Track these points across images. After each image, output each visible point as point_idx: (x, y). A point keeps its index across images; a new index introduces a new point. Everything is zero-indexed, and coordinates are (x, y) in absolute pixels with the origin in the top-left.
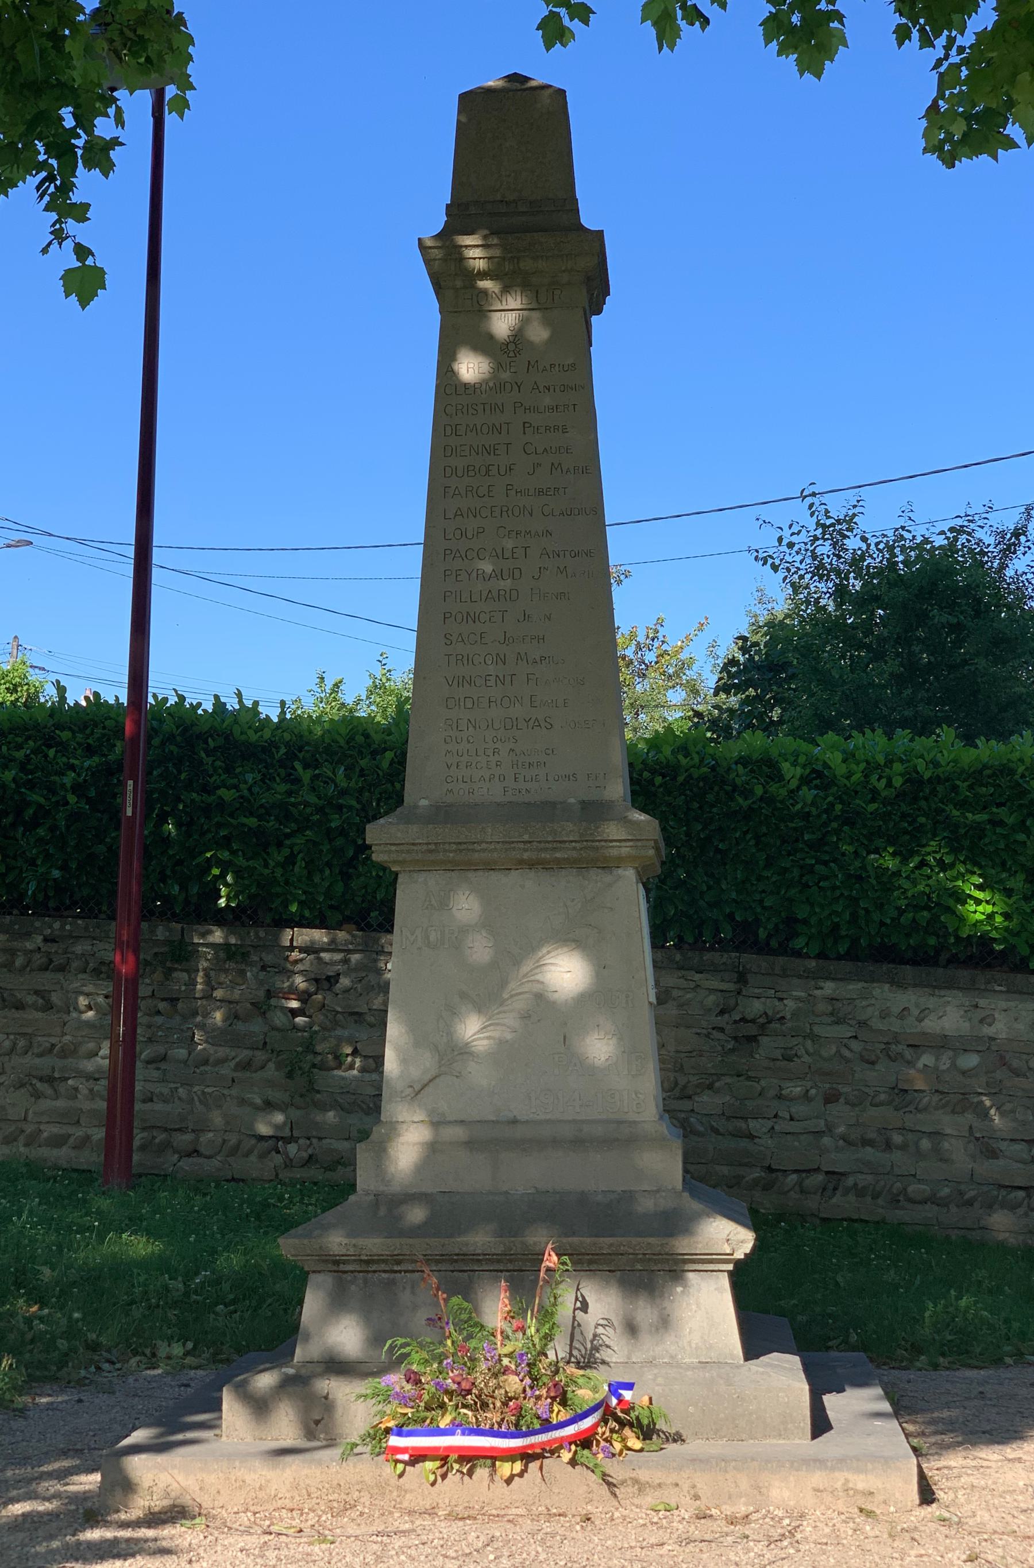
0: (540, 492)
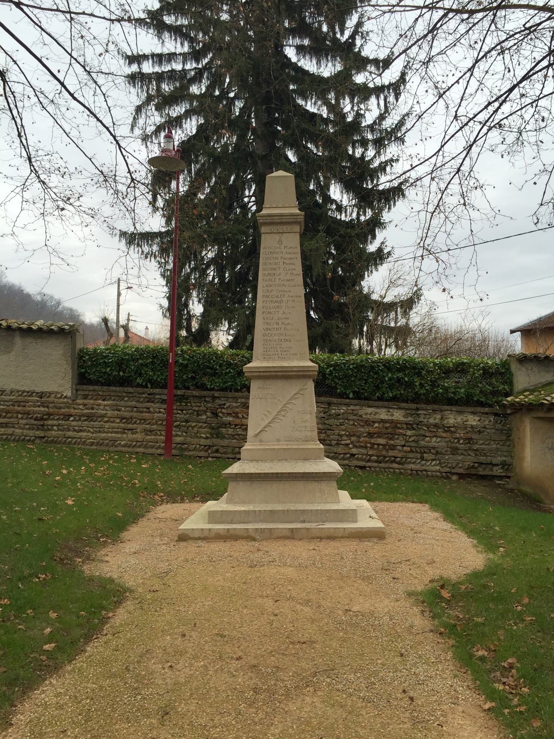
0: (288, 280)
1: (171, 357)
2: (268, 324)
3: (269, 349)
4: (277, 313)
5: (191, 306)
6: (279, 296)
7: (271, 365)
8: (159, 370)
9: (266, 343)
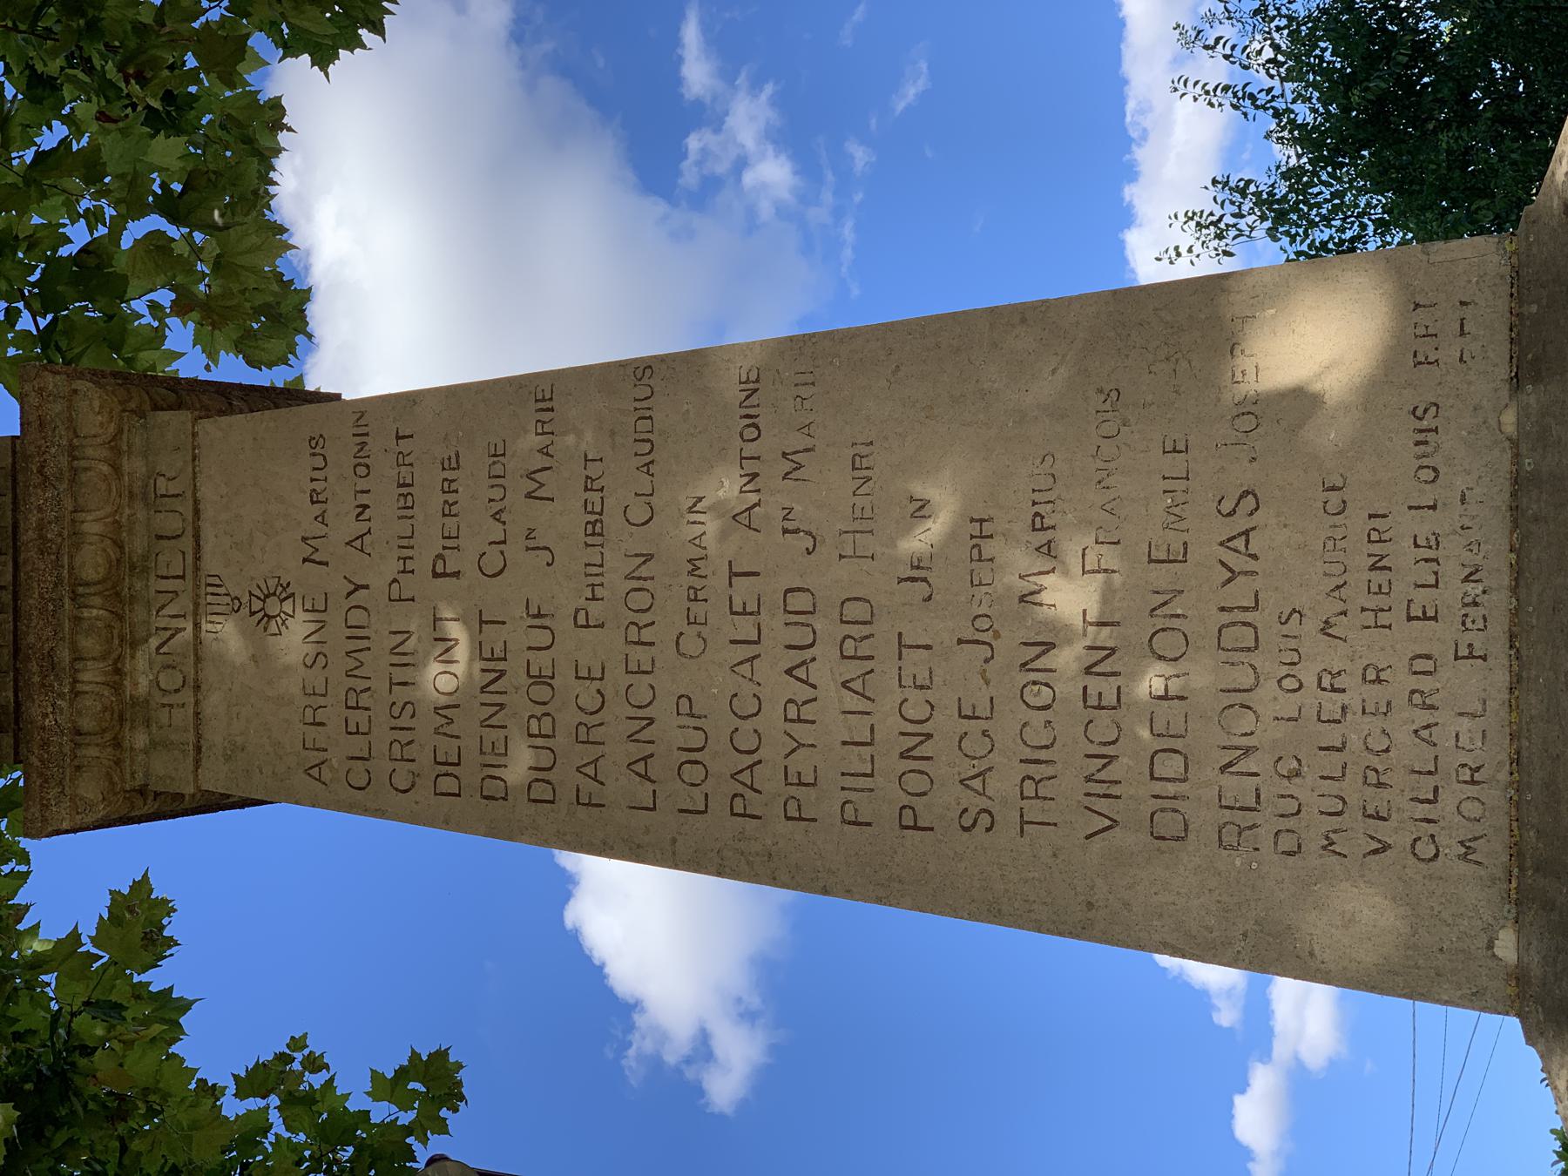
0: (595, 529)
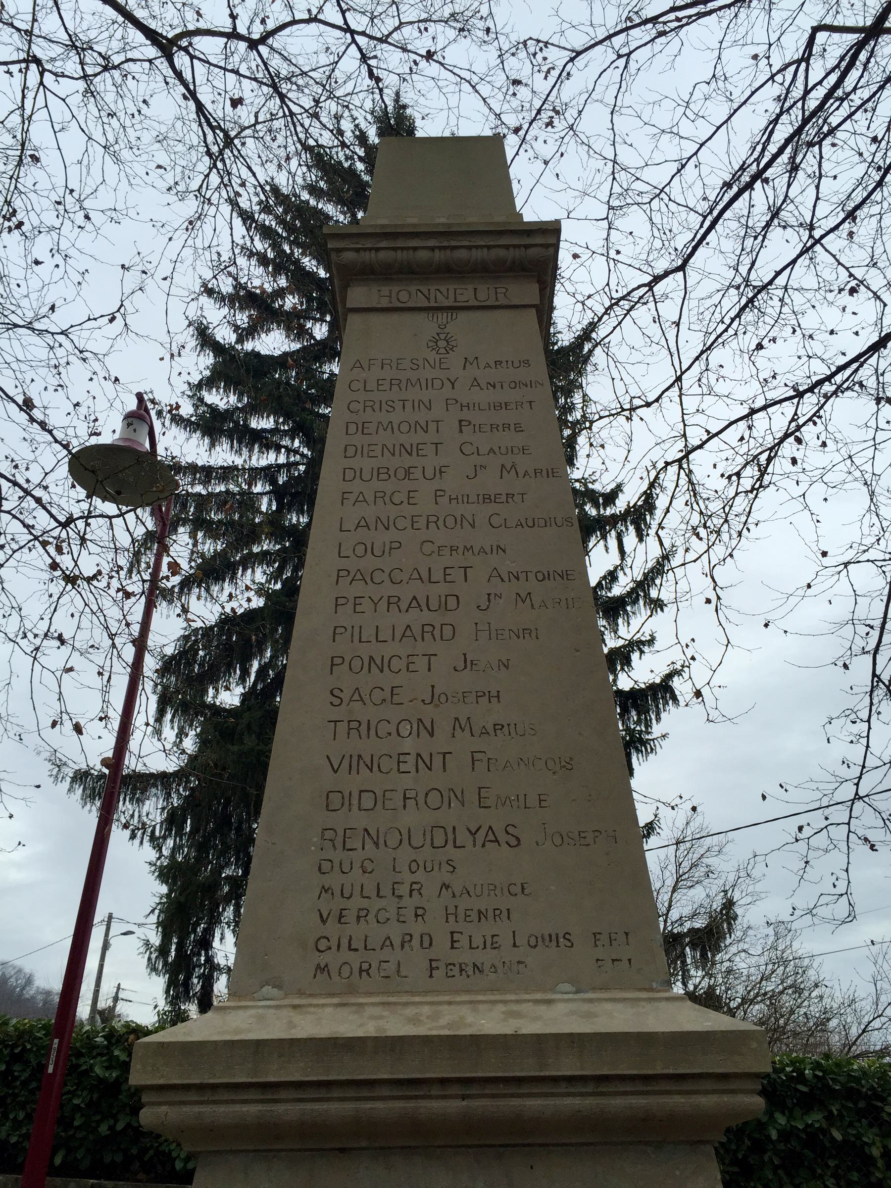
0: (487, 499)
1: (53, 1057)
2: (354, 726)
3: (357, 902)
4: (421, 663)
5: (216, 943)
6: (437, 575)
7: (369, 1029)
8: (23, 1106)
9: (337, 855)
